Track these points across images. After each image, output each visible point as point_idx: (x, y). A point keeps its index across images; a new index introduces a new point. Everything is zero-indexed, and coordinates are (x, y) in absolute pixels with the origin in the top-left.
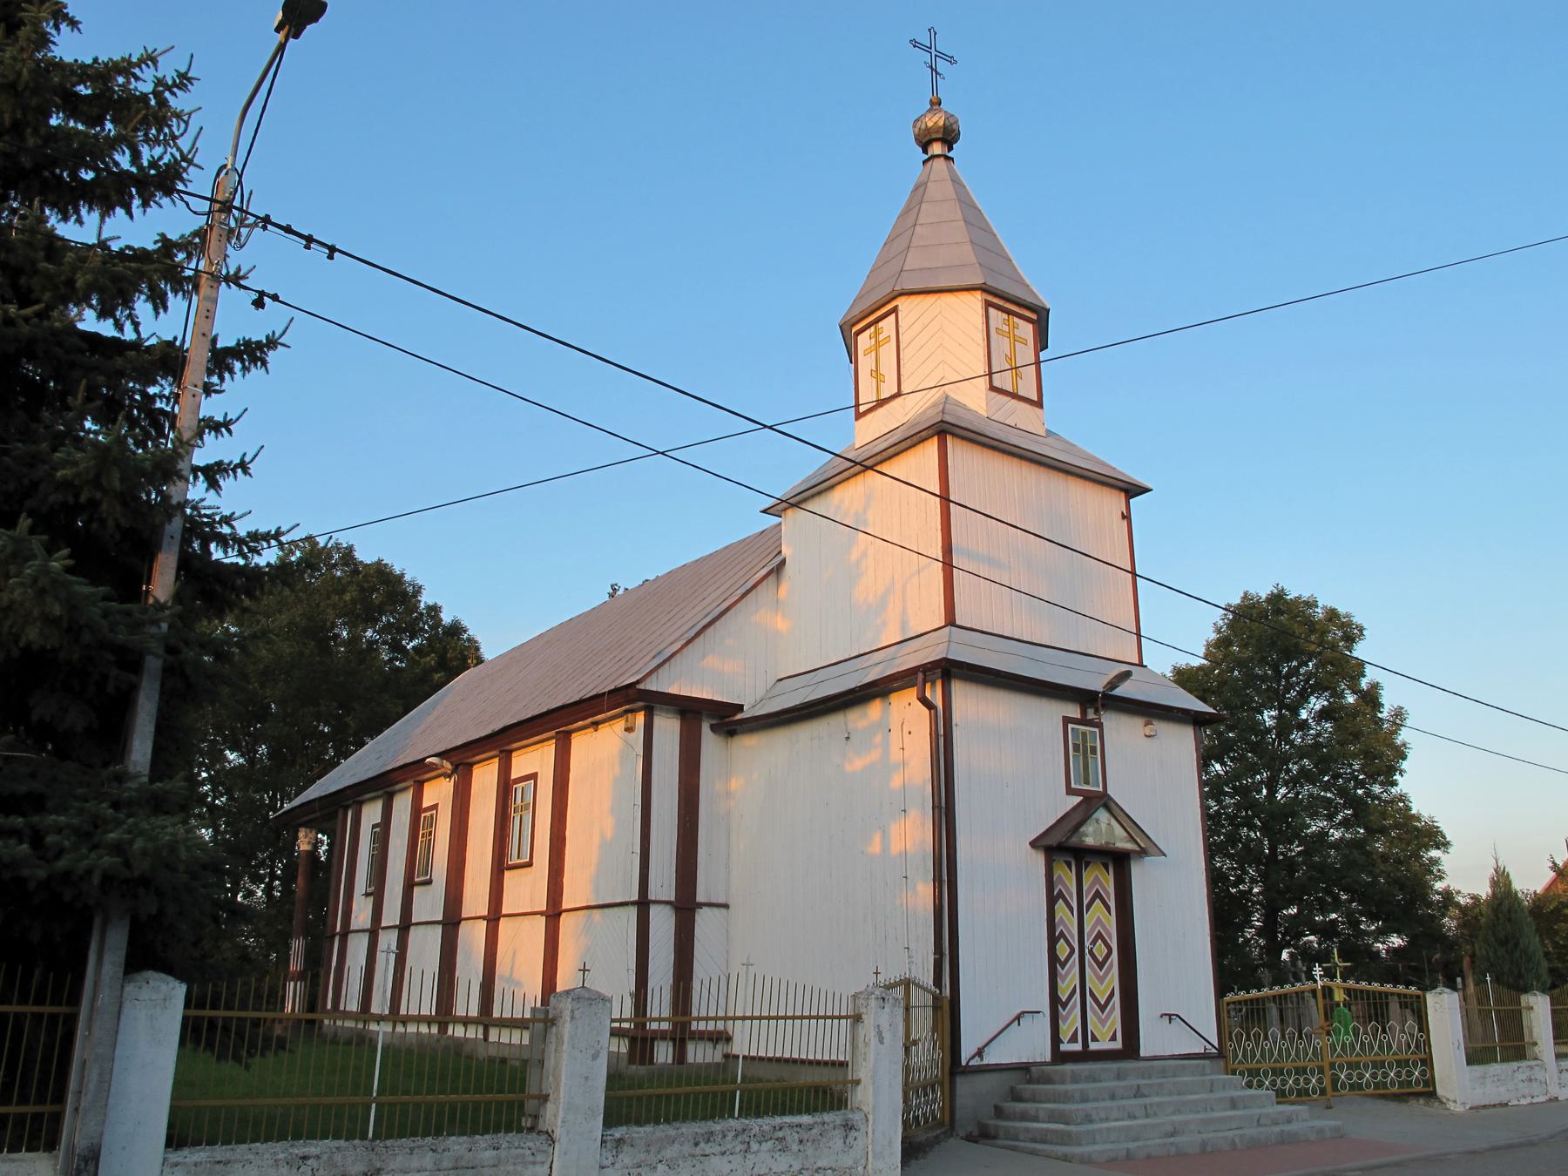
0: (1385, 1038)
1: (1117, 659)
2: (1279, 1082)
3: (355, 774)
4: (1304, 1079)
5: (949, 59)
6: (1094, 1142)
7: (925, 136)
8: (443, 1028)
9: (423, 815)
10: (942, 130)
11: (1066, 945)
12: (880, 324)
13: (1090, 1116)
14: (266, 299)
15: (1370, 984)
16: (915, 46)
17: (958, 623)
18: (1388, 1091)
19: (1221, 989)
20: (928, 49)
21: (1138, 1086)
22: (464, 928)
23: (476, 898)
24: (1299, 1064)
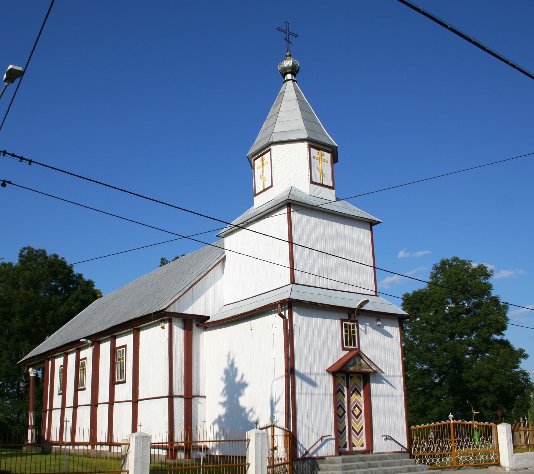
0: (471, 444)
1: (366, 293)
2: (423, 460)
3: (51, 345)
4: (434, 460)
7: (284, 71)
8: (93, 447)
9: (81, 362)
10: (291, 68)
11: (342, 410)
12: (264, 156)
14: (6, 183)
16: (279, 31)
17: (296, 282)
19: (409, 423)
20: (285, 31)
22: (99, 407)
23: (103, 395)
24: (442, 453)
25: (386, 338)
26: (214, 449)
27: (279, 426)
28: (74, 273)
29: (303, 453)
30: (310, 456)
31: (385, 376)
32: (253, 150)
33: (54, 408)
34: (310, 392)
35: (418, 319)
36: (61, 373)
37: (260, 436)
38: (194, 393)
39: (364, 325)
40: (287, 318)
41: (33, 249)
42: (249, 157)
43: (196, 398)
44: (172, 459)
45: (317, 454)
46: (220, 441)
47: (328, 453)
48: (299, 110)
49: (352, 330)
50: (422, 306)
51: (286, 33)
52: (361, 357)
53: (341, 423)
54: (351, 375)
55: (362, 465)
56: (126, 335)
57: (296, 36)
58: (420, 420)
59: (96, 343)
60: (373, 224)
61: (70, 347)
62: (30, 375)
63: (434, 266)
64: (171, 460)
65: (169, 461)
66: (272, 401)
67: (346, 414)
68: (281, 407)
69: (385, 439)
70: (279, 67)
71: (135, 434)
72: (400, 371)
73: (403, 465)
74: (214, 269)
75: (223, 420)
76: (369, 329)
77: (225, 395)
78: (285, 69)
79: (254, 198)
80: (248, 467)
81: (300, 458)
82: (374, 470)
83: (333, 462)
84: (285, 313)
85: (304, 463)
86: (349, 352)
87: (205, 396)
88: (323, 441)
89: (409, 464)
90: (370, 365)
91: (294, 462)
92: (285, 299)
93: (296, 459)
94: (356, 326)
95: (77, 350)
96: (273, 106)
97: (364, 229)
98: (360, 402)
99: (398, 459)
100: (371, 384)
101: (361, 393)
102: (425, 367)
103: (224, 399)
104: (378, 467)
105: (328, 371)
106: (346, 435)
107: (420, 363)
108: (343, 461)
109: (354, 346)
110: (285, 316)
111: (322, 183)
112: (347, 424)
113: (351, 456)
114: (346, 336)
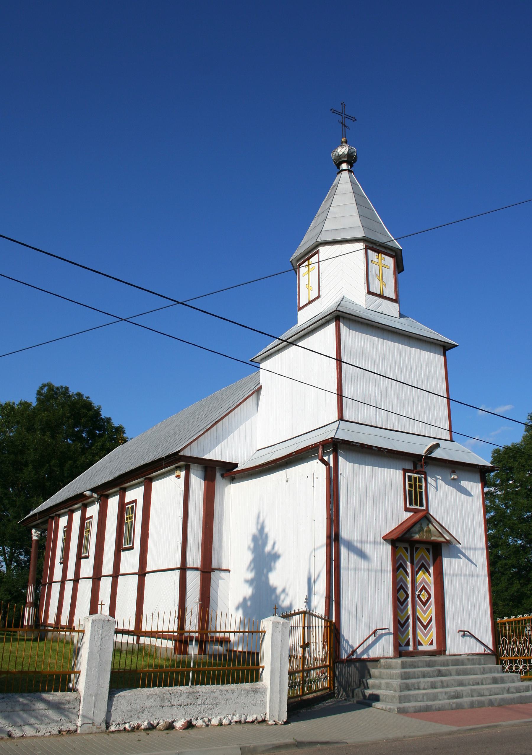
2: (514, 667)
6: (409, 701)
9: (86, 521)
10: (347, 156)
11: (404, 593)
15: (503, 619)
16: (333, 113)
17: (345, 418)
20: (340, 114)
22: (60, 579)
23: (107, 568)
25: (463, 496)
26: (237, 644)
27: (317, 615)
28: (101, 417)
29: (348, 652)
30: (359, 657)
31: (462, 548)
32: (297, 253)
33: (54, 580)
34: (360, 566)
35: (511, 482)
36: (64, 536)
37: (280, 627)
38: (214, 565)
39: (434, 479)
40: (332, 465)
41: (54, 386)
42: (293, 262)
43: (216, 571)
44: (180, 654)
45: (368, 655)
46: (244, 632)
47: (383, 654)
48: (355, 204)
49: (418, 484)
50: (516, 464)
51: (342, 115)
52: (430, 522)
53: (402, 611)
54: (417, 545)
55: (428, 673)
56: (137, 487)
57: (354, 119)
58: (515, 611)
59: (103, 497)
60: (446, 348)
61: (73, 503)
62: (32, 538)
63: (529, 416)
64: (178, 656)
65: (178, 657)
66: (309, 579)
67: (410, 599)
68: (321, 587)
69: (462, 636)
70: (333, 155)
71: (94, 617)
72: (482, 542)
73: (486, 673)
74: (246, 403)
75: (249, 603)
76: (441, 483)
77: (252, 571)
78: (339, 157)
79: (298, 312)
80: (262, 672)
81: (344, 659)
82: (445, 681)
83: (389, 667)
84: (329, 459)
85: (350, 668)
86: (413, 514)
87: (229, 569)
88: (377, 636)
89: (494, 672)
90: (442, 533)
91: (336, 665)
92: (328, 439)
93: (339, 660)
94: (423, 479)
95: (83, 507)
96: (324, 201)
97: (435, 353)
98: (429, 584)
99: (479, 664)
100: (443, 558)
101: (430, 571)
102: (520, 542)
103: (250, 575)
104: (451, 675)
105: (385, 538)
106: (410, 628)
107: (514, 538)
108: (404, 665)
109: (420, 506)
110: (329, 463)
111: (382, 294)
112: (410, 613)
113: (415, 659)
114: (410, 492)
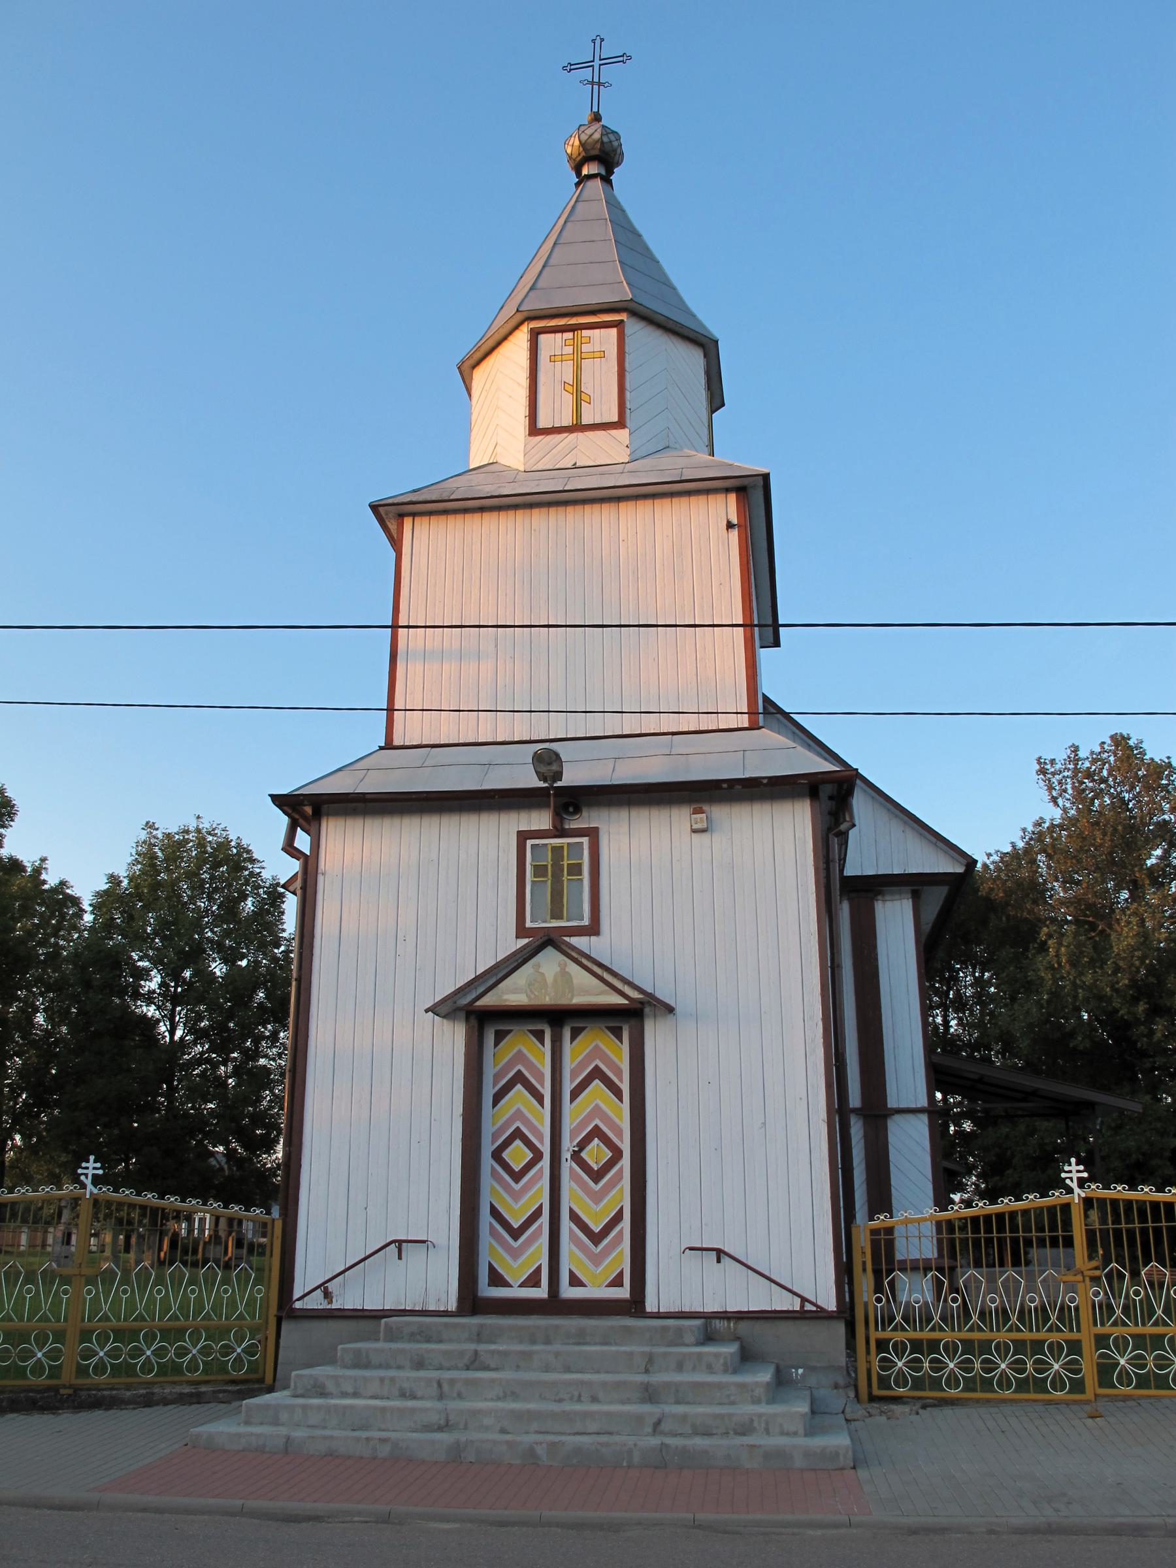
5: (621, 59)
13: (323, 1386)
18: (88, 1381)
21: (476, 1352)
24: (1026, 1335)
